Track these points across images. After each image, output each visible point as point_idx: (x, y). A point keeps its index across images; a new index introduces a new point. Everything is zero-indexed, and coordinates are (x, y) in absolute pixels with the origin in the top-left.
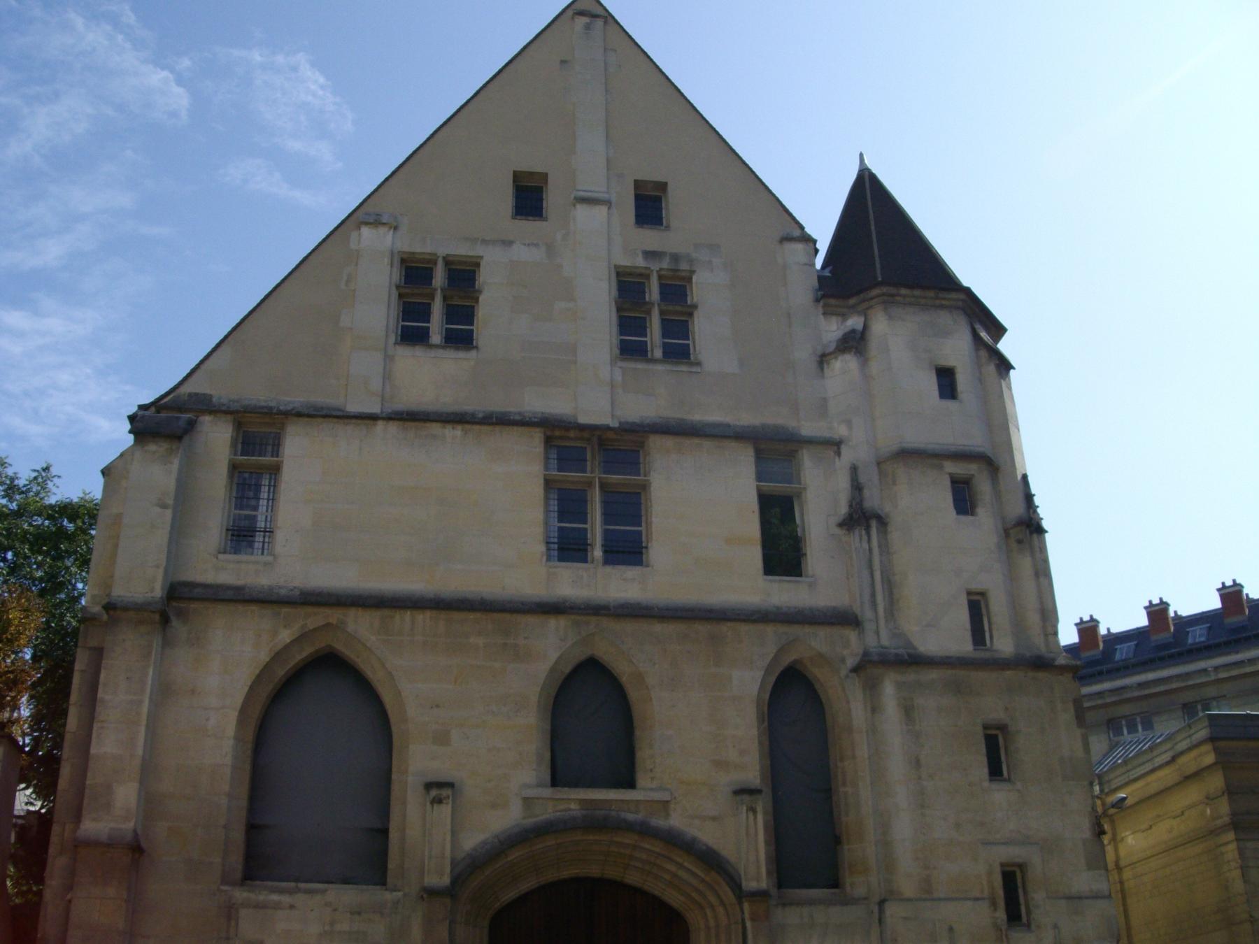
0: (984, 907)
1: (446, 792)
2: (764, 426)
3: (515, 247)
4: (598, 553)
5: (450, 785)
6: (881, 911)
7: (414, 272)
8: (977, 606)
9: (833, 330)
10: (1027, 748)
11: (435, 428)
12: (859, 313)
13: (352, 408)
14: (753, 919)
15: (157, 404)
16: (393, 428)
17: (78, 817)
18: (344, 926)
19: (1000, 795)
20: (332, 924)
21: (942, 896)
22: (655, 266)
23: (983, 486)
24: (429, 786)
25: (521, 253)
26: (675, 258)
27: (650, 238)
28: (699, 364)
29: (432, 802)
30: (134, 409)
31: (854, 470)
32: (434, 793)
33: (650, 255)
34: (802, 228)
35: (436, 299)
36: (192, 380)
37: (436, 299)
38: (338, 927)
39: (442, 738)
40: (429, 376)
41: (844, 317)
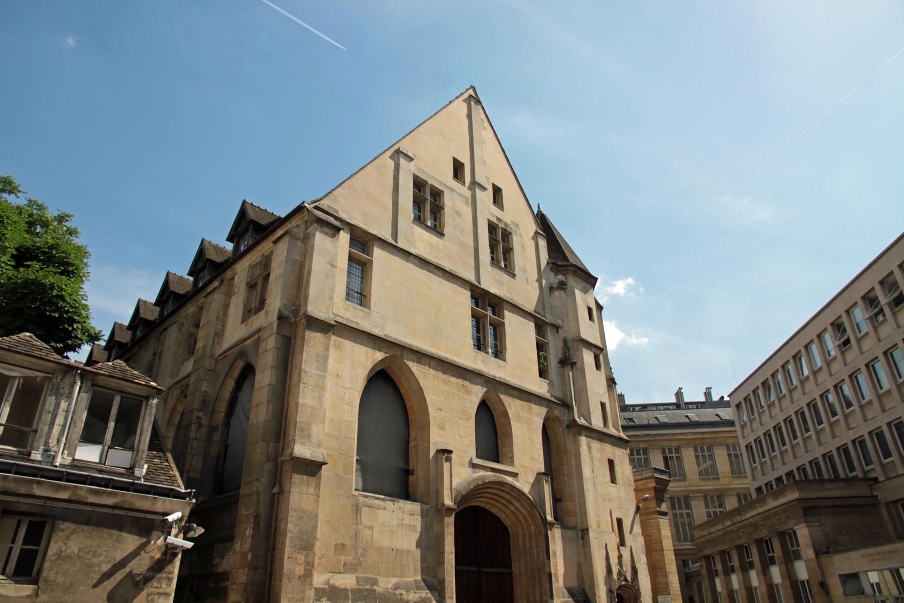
18: (407, 522)
20: (402, 520)
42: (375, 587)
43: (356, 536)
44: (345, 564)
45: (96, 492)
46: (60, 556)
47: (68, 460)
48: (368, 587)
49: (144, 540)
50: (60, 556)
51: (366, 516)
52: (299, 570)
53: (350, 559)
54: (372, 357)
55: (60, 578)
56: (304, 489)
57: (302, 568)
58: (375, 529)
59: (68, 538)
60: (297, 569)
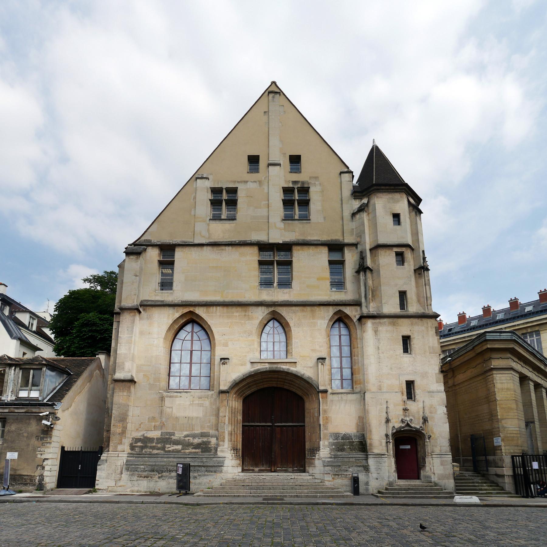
0: (399, 395)
1: (226, 361)
2: (332, 240)
3: (248, 183)
4: (275, 284)
5: (228, 359)
6: (364, 396)
7: (216, 191)
8: (403, 295)
9: (356, 204)
10: (415, 343)
11: (223, 248)
12: (366, 197)
13: (197, 242)
14: (322, 398)
15: (134, 244)
16: (209, 248)
17: (114, 372)
18: (197, 402)
19: (406, 358)
20: (193, 401)
21: (385, 391)
22: (296, 187)
23: (408, 255)
24: (221, 359)
25: (251, 185)
26: (303, 183)
27: (295, 177)
28: (310, 220)
29: (222, 364)
30: (126, 246)
31: (361, 252)
32: (223, 361)
33: (295, 182)
34: (348, 168)
35: (224, 200)
36: (145, 235)
37: (224, 200)
38: (195, 402)
39: (226, 345)
40: (220, 231)
41: (361, 199)
42: (172, 437)
43: (161, 412)
44: (154, 426)
45: (17, 408)
46: (9, 431)
47: (14, 398)
48: (168, 437)
49: (513, 492)
50: (9, 431)
51: (168, 402)
52: (119, 430)
53: (157, 424)
54: (331, 311)
55: (10, 439)
56: (121, 394)
57: (120, 430)
58: (174, 408)
59: (11, 425)
60: (118, 430)
